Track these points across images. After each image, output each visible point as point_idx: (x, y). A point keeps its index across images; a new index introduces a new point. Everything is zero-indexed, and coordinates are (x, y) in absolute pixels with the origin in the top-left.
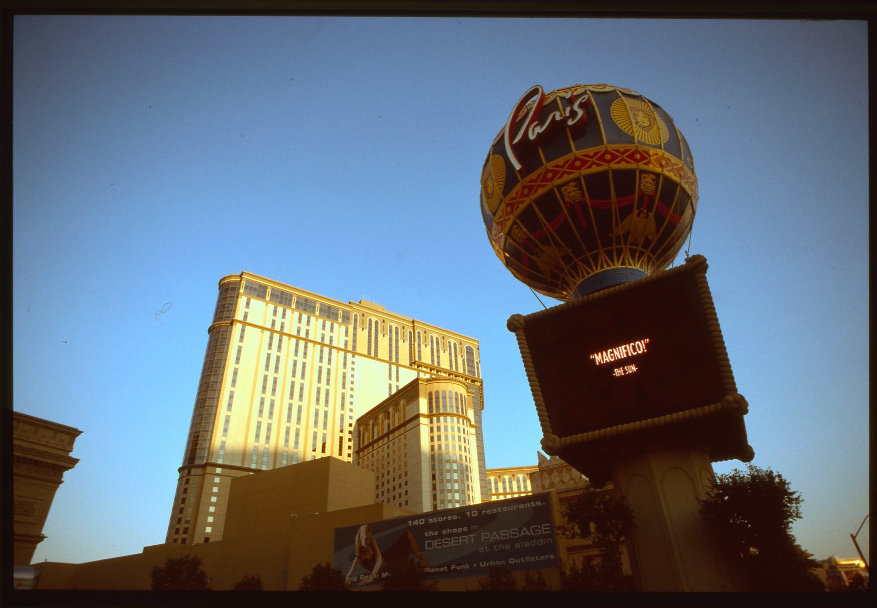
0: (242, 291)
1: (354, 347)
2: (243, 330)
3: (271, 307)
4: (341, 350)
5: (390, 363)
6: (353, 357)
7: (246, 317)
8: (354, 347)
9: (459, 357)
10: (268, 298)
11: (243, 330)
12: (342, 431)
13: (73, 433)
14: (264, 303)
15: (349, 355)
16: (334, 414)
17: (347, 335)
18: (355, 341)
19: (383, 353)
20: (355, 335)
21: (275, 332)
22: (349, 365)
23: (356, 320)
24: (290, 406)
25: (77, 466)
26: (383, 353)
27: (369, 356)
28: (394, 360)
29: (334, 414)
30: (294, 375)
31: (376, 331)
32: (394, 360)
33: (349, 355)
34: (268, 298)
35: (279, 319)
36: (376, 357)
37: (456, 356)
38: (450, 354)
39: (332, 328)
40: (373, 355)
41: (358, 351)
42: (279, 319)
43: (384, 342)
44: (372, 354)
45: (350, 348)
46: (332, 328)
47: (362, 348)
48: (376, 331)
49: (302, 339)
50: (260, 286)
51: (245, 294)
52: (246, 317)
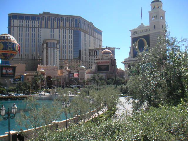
10: (18, 19)
17: (39, 23)
18: (41, 24)
22: (40, 31)
38: (64, 22)
44: (46, 27)
45: (40, 26)
47: (43, 26)
49: (27, 27)
50: (16, 16)
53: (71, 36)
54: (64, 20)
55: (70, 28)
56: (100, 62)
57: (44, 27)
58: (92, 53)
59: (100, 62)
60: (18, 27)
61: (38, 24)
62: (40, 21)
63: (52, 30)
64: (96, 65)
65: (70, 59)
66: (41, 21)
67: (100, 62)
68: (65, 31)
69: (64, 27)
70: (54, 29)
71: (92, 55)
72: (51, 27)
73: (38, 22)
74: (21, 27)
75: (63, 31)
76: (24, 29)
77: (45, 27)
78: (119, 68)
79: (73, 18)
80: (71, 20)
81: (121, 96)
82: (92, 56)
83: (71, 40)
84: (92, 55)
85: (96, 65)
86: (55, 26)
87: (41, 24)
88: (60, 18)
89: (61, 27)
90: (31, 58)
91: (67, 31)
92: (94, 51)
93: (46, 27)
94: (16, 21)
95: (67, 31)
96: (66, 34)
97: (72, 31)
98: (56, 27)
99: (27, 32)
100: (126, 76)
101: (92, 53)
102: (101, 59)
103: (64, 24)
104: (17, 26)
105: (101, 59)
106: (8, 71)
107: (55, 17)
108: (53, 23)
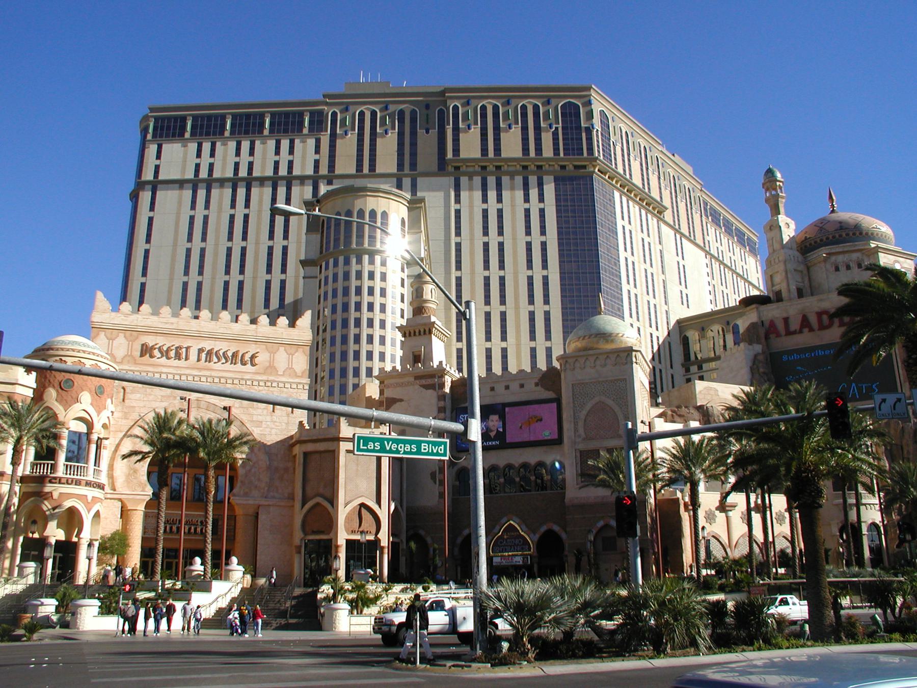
17: (317, 151)
38: (525, 129)
45: (324, 170)
50: (176, 118)
53: (542, 212)
55: (528, 171)
56: (795, 325)
59: (786, 320)
60: (181, 184)
61: (311, 157)
62: (325, 139)
64: (758, 348)
67: (795, 325)
73: (311, 142)
74: (200, 184)
78: (821, 510)
80: (413, 120)
81: (90, 392)
83: (544, 245)
85: (758, 348)
88: (456, 108)
93: (366, 170)
94: (172, 149)
96: (522, 239)
98: (434, 167)
102: (800, 293)
104: (177, 176)
105: (800, 293)
107: (427, 107)
108: (414, 144)
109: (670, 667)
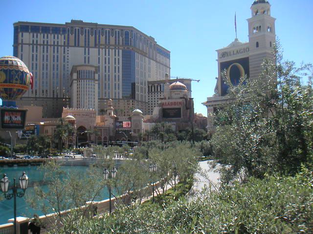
0: (19, 30)
1: (68, 43)
2: (22, 47)
3: (31, 34)
4: (42, 45)
5: (85, 47)
6: (68, 48)
7: (22, 41)
8: (68, 43)
9: (121, 37)
10: (30, 31)
11: (22, 47)
12: (53, 88)
13: (276, 19)
14: (28, 34)
15: (66, 48)
16: (102, 66)
17: (64, 39)
18: (68, 41)
19: (82, 43)
20: (68, 38)
21: (34, 44)
22: (66, 52)
23: (68, 31)
24: (115, 59)
25: (247, 18)
26: (82, 43)
27: (75, 46)
28: (87, 45)
29: (102, 66)
30: (105, 55)
31: (78, 33)
32: (87, 45)
33: (66, 48)
34: (30, 31)
35: (35, 39)
36: (78, 46)
37: (119, 37)
38: (106, 37)
39: (37, 36)
40: (77, 45)
41: (70, 44)
42: (35, 39)
43: (82, 38)
44: (77, 45)
45: (66, 44)
46: (37, 36)
47: (72, 43)
48: (78, 33)
49: (45, 45)
50: (26, 26)
51: (21, 31)
52: (22, 41)
53: (119, 59)
54: (106, 33)
55: (116, 46)
56: (167, 104)
57: (74, 45)
58: (153, 88)
59: (166, 103)
60: (29, 44)
61: (63, 40)
62: (66, 35)
63: (87, 49)
64: (161, 108)
65: (117, 98)
66: (68, 35)
67: (167, 104)
68: (109, 51)
69: (107, 45)
70: (90, 49)
71: (153, 90)
72: (85, 44)
73: (63, 36)
74: (34, 44)
75: (105, 51)
76: (40, 48)
77: (75, 45)
78: (197, 114)
79: (122, 30)
80: (119, 34)
81: (202, 160)
82: (153, 94)
83: (119, 67)
84: (153, 90)
85: (161, 108)
86: (92, 43)
87: (68, 41)
88: (99, 31)
89: (101, 45)
90: (52, 96)
91: (112, 52)
92: (156, 85)
93: (77, 45)
94: (26, 35)
95: (112, 52)
96: (110, 57)
97: (121, 51)
98: (94, 46)
99: (45, 54)
100: (210, 126)
101: (153, 88)
102: (169, 98)
103: (106, 39)
104: (28, 43)
105: (169, 98)
106: (14, 118)
107: (92, 29)
108: (89, 39)
109: (220, 67)
